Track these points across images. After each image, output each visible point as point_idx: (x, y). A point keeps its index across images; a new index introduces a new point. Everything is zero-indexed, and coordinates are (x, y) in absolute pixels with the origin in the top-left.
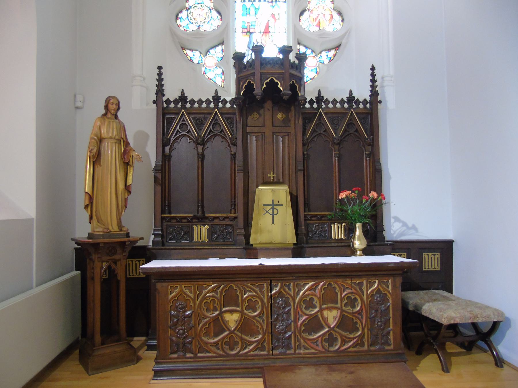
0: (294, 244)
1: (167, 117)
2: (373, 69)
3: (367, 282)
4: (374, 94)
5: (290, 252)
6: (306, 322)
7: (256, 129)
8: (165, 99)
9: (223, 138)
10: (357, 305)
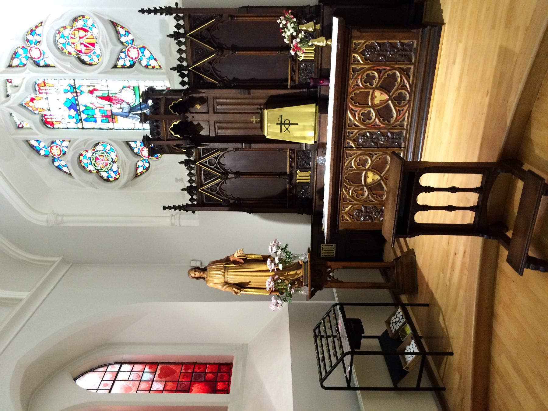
0: (316, 105)
1: (205, 201)
2: (143, 11)
3: (353, 64)
4: (168, 11)
5: (322, 115)
6: (382, 119)
7: (212, 128)
8: (190, 203)
9: (221, 157)
10: (372, 73)
